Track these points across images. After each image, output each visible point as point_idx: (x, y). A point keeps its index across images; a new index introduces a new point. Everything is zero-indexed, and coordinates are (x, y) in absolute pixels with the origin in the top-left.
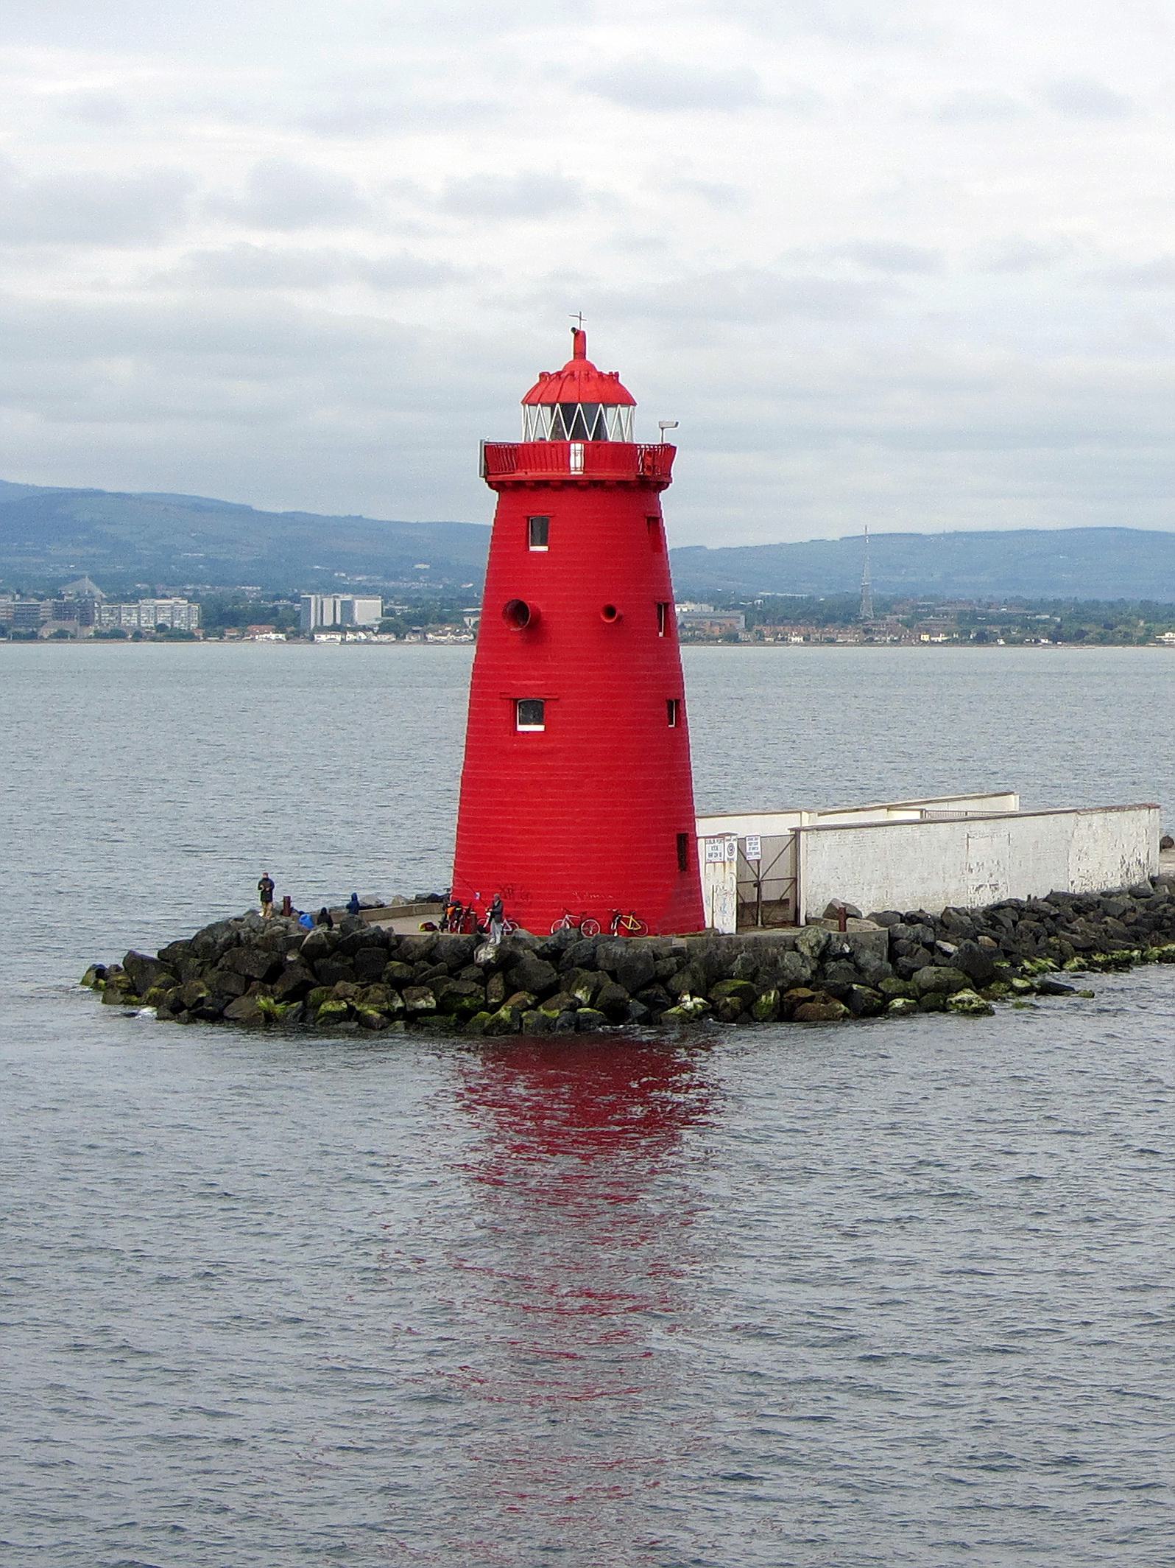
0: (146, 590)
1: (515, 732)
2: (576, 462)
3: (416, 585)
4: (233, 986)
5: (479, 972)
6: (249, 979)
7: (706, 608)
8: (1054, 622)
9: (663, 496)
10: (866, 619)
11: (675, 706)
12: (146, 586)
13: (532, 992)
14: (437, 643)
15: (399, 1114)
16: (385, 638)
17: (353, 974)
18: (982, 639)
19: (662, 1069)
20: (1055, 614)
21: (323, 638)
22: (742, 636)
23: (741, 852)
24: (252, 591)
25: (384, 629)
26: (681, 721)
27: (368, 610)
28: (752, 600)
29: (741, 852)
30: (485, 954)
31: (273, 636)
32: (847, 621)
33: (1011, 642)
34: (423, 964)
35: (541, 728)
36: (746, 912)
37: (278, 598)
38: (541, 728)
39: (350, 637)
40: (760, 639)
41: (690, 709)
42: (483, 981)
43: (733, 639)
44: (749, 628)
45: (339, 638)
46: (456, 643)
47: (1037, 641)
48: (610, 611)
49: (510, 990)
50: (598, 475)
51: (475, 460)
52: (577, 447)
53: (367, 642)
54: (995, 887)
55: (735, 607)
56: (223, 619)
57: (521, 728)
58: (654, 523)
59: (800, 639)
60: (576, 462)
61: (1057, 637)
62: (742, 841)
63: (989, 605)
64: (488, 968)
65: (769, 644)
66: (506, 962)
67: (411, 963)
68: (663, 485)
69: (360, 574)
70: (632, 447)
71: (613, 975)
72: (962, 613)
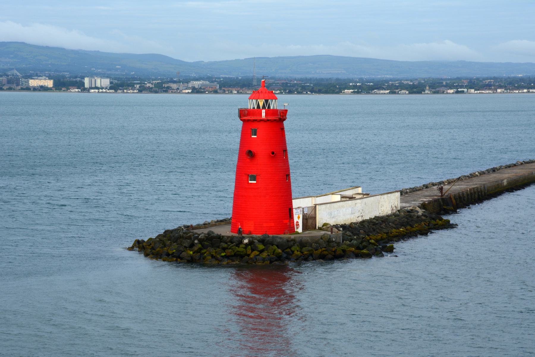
0: (34, 74)
1: (249, 183)
2: (263, 114)
3: (117, 73)
4: (181, 249)
5: (244, 246)
6: (185, 247)
7: (207, 82)
8: (311, 86)
9: (284, 122)
10: (255, 85)
11: (288, 176)
12: (33, 72)
13: (258, 251)
14: (127, 92)
15: (216, 291)
16: (111, 91)
17: (212, 246)
18: (290, 92)
19: (285, 269)
20: (311, 83)
21: (92, 91)
22: (219, 91)
23: (303, 212)
24: (67, 74)
25: (111, 88)
26: (289, 180)
27: (106, 82)
28: (220, 78)
29: (303, 212)
30: (246, 241)
31: (77, 90)
32: (249, 86)
33: (299, 93)
34: (229, 244)
35: (255, 182)
36: (305, 228)
37: (76, 77)
38: (255, 182)
39: (101, 90)
40: (224, 92)
41: (291, 175)
42: (246, 248)
43: (216, 92)
44: (220, 88)
45: (97, 91)
46: (133, 93)
47: (307, 93)
48: (273, 153)
49: (253, 250)
50: (269, 118)
51: (237, 112)
52: (264, 111)
53: (106, 92)
54: (362, 216)
55: (215, 81)
56: (61, 84)
57: (250, 182)
58: (283, 129)
59: (236, 92)
60: (263, 114)
61: (313, 91)
62: (303, 208)
63: (291, 81)
64: (246, 244)
65: (227, 94)
66: (251, 243)
67: (226, 243)
68: (285, 120)
69: (100, 69)
70: (277, 110)
71: (277, 246)
72: (283, 84)
